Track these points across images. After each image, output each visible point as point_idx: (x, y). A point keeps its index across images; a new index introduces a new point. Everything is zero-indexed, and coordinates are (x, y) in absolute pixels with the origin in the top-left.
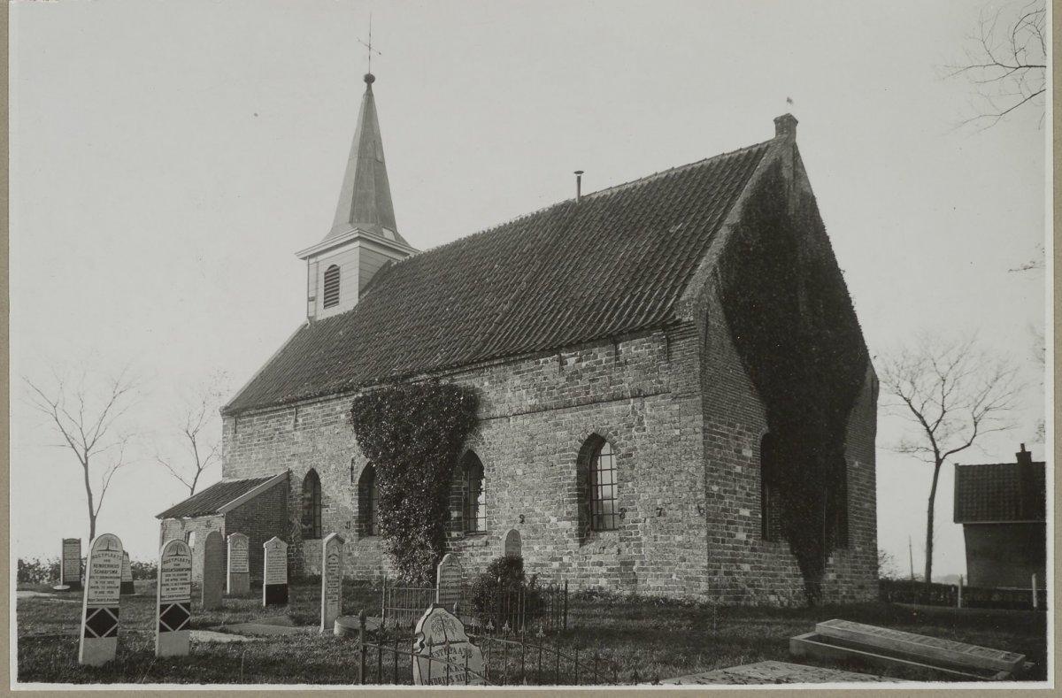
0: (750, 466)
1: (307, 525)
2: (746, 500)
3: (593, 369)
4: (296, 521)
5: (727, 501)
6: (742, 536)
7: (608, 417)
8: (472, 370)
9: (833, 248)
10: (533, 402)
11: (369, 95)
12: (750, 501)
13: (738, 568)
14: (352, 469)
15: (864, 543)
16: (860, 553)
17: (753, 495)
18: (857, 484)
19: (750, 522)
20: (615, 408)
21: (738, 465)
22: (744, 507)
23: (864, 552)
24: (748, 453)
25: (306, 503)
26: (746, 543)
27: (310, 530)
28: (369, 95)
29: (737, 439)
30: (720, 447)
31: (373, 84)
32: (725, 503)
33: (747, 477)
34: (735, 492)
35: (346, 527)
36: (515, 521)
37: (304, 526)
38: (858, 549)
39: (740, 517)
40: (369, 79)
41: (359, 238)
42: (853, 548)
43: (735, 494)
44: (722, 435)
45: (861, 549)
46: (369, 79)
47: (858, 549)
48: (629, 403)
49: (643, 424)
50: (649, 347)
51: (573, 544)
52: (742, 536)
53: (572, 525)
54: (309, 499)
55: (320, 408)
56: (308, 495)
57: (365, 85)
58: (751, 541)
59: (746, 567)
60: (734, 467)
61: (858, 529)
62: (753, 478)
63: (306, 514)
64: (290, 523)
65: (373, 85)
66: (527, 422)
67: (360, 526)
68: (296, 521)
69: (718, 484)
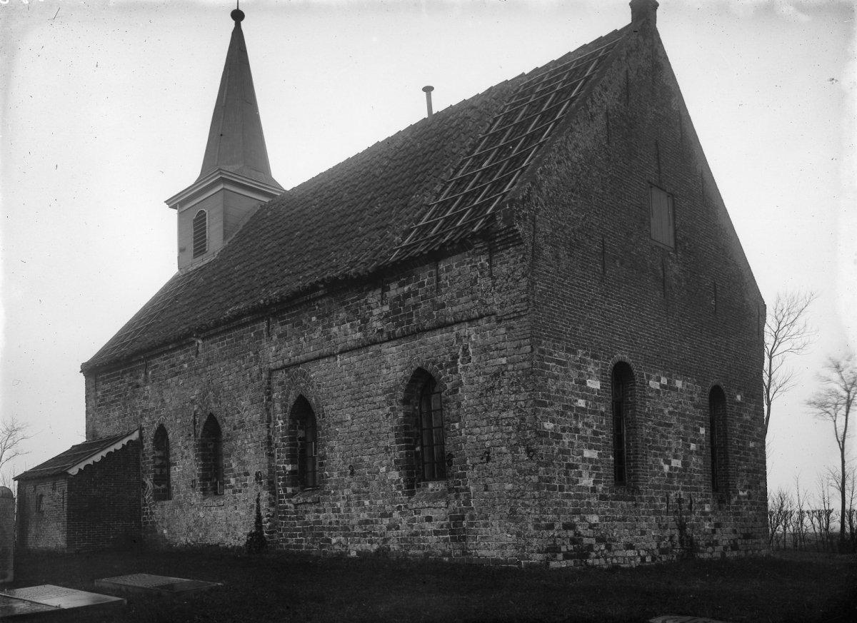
0: (597, 399)
1: (160, 485)
2: (593, 440)
3: (416, 293)
4: (149, 482)
5: (566, 441)
6: (587, 481)
7: (433, 345)
8: (300, 305)
9: (604, 35)
10: (359, 335)
11: (238, 38)
12: (599, 440)
13: (583, 519)
14: (195, 423)
15: (750, 487)
16: (745, 497)
17: (601, 434)
18: (739, 420)
19: (599, 465)
20: (438, 336)
21: (582, 398)
22: (590, 448)
23: (749, 497)
24: (594, 384)
25: (158, 462)
26: (594, 490)
27: (164, 490)
28: (238, 38)
29: (579, 367)
30: (556, 378)
31: (242, 22)
32: (564, 443)
33: (594, 412)
34: (577, 430)
35: (192, 486)
36: (345, 474)
37: (157, 487)
38: (741, 493)
39: (584, 460)
40: (238, 15)
41: (223, 180)
42: (736, 492)
43: (579, 433)
44: (559, 362)
45: (745, 493)
46: (238, 15)
47: (741, 493)
48: (452, 331)
49: (468, 353)
50: (471, 262)
51: (400, 495)
52: (587, 481)
53: (401, 475)
54: (160, 458)
55: (165, 359)
56: (158, 454)
57: (233, 23)
58: (600, 487)
59: (594, 519)
60: (576, 401)
61: (743, 471)
62: (602, 414)
63: (158, 473)
64: (144, 484)
65: (243, 23)
66: (354, 359)
67: (203, 485)
68: (149, 482)
69: (553, 421)
